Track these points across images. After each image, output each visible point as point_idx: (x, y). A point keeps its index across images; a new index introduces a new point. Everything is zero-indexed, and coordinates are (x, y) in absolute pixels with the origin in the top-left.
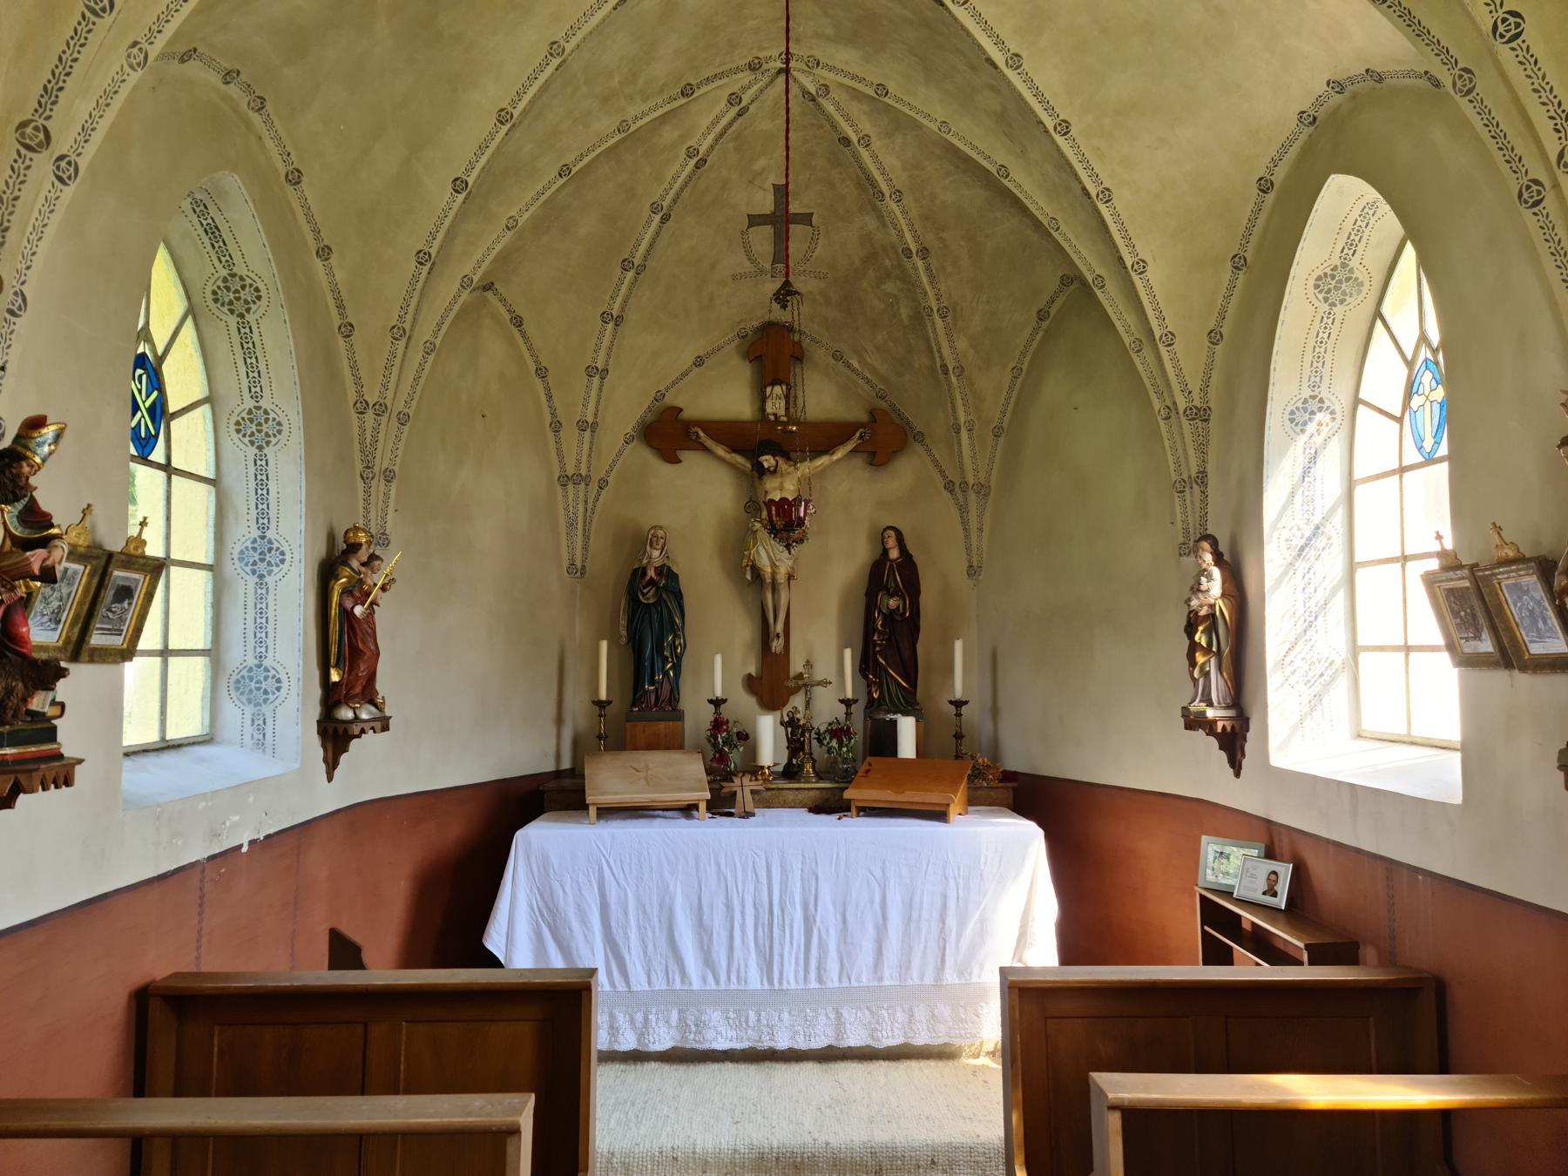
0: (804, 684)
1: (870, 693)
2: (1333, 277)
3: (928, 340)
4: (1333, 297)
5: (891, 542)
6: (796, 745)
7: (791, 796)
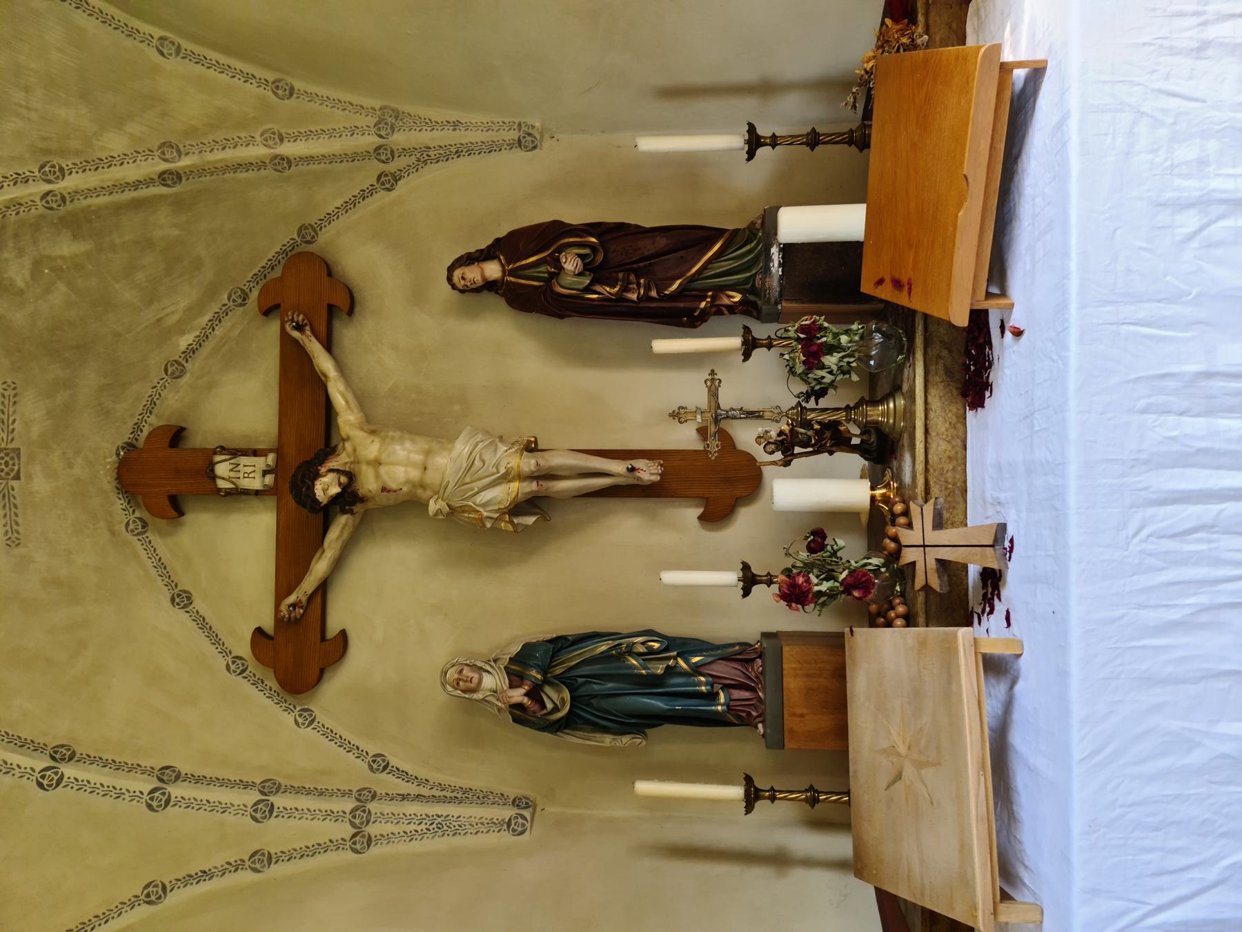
0: (717, 422)
1: (732, 309)
3: (118, 208)
5: (473, 274)
6: (829, 439)
7: (940, 447)
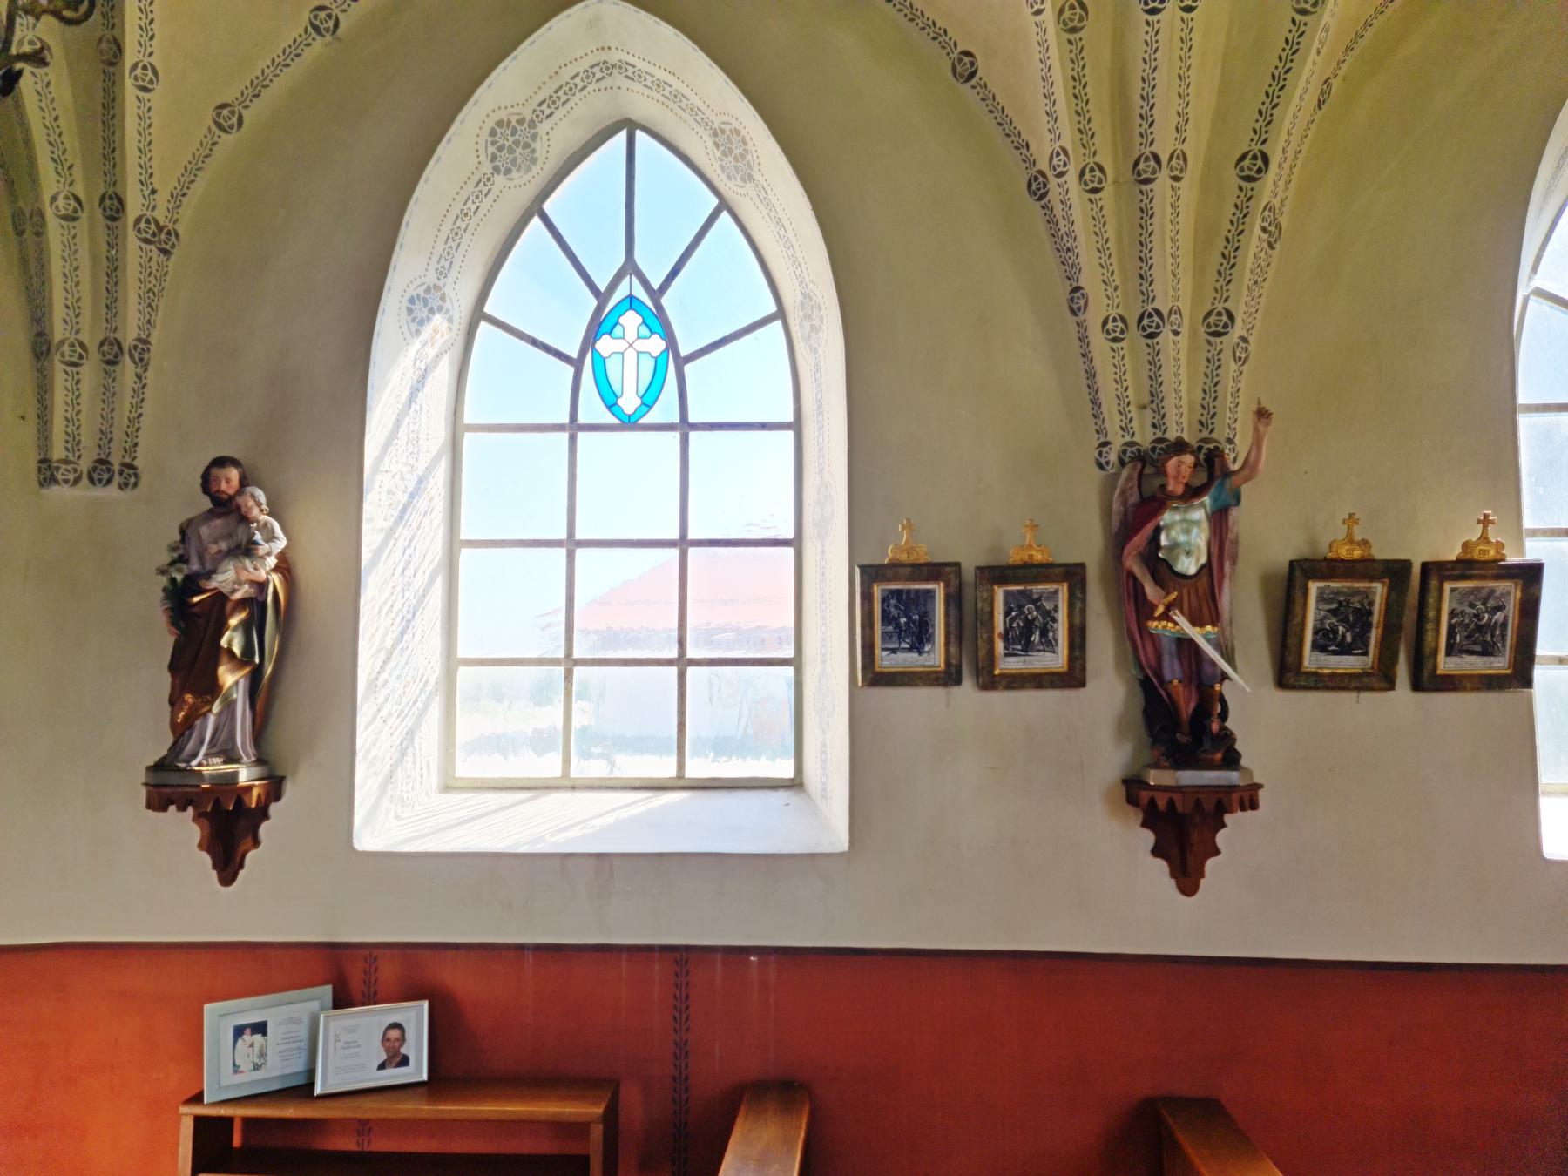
2: (514, 132)
4: (504, 159)
